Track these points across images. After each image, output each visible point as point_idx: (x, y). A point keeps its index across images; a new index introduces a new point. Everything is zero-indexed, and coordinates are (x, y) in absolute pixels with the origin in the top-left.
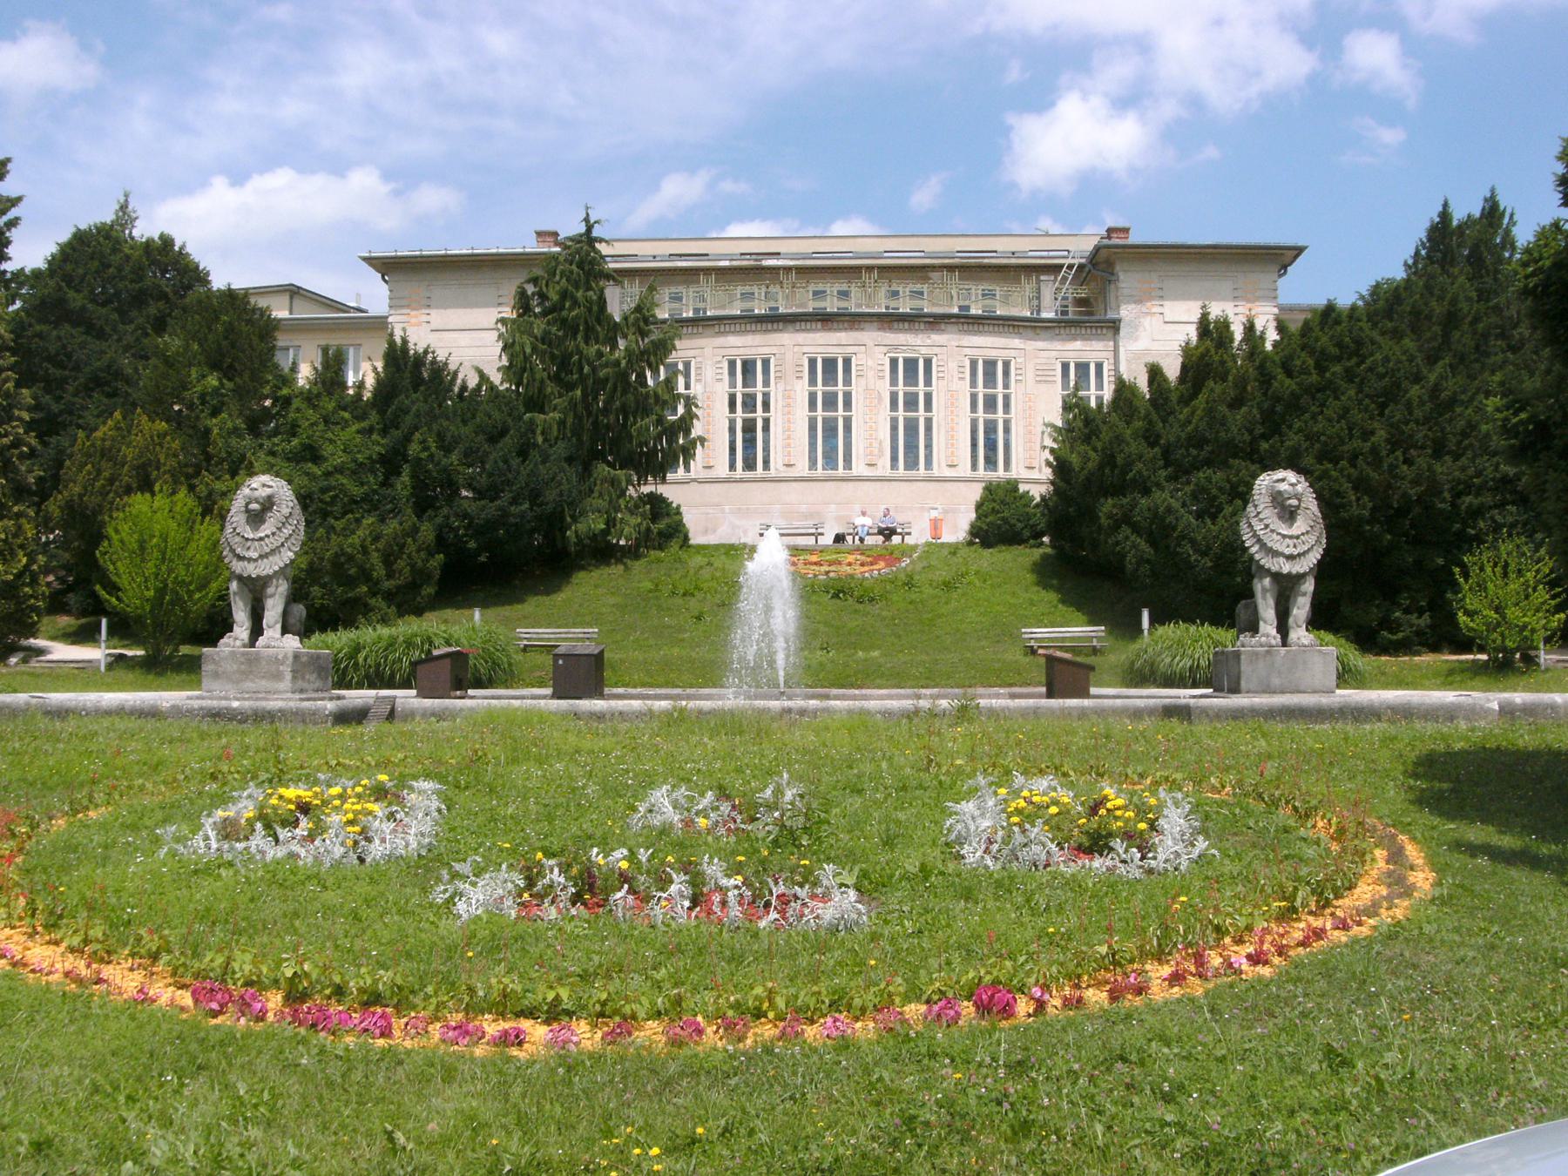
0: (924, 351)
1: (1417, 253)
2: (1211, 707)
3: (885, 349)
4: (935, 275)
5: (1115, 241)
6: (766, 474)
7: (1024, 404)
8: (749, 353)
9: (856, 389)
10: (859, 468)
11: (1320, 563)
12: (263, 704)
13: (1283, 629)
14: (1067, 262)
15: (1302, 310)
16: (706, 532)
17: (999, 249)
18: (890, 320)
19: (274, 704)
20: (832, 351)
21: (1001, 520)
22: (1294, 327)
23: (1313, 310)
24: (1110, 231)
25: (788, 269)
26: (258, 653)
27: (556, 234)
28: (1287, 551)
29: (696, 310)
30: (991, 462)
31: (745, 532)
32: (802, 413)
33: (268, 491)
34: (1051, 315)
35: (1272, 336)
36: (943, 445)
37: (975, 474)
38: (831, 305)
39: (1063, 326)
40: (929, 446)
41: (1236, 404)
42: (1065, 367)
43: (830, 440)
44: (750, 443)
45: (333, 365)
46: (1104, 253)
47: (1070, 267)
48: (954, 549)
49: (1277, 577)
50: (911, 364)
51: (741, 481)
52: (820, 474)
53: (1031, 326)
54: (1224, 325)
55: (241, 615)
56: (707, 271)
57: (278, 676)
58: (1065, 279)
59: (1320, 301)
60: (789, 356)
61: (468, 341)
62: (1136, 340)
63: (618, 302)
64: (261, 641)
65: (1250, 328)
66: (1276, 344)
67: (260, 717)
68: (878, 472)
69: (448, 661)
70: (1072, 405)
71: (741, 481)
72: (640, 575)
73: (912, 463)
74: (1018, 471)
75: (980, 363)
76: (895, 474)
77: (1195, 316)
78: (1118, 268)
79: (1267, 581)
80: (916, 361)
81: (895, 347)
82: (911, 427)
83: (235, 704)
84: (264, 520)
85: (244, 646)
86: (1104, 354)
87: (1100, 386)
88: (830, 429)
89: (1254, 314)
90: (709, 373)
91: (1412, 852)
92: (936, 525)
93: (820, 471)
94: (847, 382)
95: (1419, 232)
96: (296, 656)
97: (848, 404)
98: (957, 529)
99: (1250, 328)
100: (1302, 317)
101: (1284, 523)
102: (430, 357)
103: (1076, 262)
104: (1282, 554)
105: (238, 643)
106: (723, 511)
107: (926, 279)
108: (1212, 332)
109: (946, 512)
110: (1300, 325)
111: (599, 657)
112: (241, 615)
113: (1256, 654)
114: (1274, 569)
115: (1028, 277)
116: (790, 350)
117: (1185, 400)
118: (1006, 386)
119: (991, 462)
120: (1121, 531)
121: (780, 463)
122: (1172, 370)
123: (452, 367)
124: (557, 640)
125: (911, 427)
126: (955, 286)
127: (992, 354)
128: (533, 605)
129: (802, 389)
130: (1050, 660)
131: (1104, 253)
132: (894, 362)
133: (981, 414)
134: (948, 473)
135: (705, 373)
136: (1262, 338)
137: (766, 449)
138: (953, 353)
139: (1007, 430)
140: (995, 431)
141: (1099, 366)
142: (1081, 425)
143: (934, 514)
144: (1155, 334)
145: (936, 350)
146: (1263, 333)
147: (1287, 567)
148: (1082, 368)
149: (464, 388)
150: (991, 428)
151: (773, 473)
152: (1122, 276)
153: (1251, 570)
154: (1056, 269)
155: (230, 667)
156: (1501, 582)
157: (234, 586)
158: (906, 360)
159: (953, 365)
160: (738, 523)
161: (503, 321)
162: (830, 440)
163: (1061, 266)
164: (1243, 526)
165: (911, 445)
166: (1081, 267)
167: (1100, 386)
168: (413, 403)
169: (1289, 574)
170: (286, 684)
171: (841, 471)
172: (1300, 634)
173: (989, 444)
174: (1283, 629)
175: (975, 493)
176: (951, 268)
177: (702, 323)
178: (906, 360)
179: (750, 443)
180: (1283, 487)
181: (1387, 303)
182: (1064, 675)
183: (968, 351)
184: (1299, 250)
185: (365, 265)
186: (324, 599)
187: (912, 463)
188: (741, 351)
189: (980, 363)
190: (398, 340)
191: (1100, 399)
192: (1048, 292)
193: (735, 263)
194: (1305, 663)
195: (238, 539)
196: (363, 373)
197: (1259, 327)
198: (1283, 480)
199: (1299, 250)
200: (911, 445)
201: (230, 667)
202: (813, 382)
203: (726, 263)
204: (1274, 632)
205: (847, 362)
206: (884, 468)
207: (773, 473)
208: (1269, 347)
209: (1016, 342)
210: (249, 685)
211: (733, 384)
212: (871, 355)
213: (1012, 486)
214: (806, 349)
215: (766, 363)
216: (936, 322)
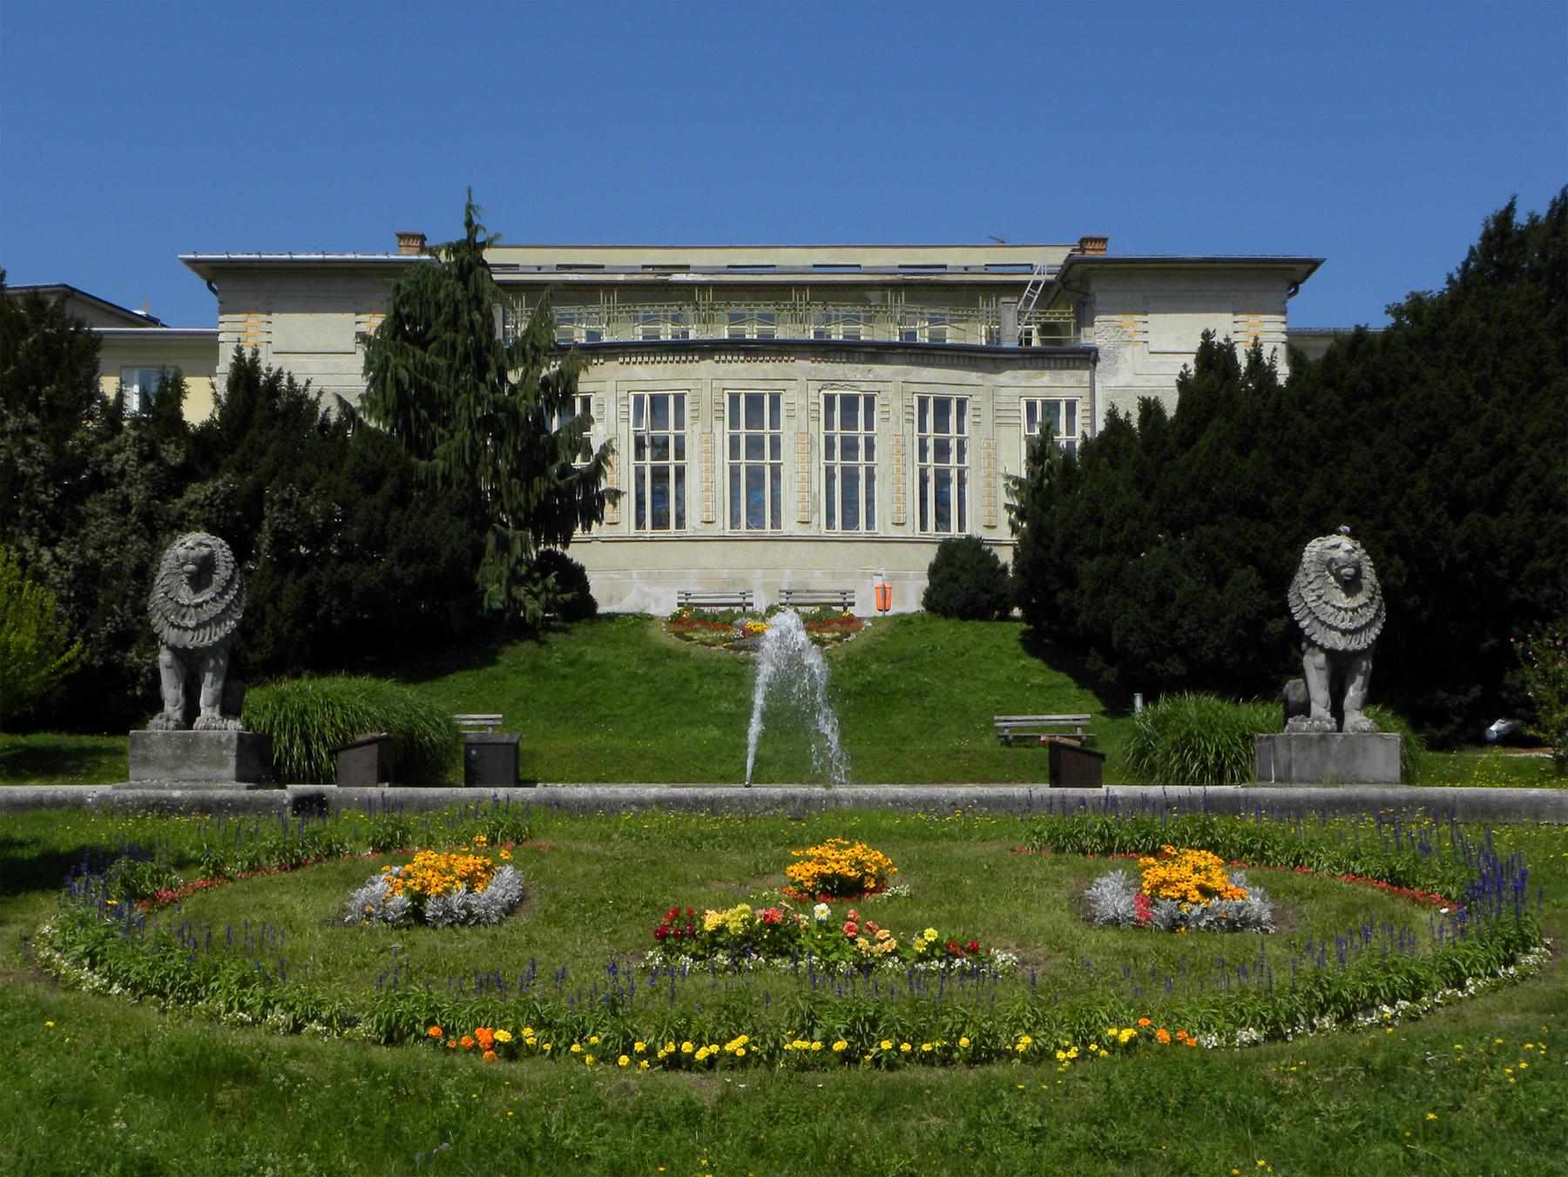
0: (864, 387)
1: (1466, 264)
2: (1262, 797)
3: (819, 385)
4: (874, 295)
5: (1090, 254)
6: (680, 532)
7: (990, 447)
8: (660, 388)
9: (787, 430)
10: (789, 526)
11: (1380, 639)
12: (211, 793)
13: (1337, 711)
14: (1032, 278)
15: (1322, 335)
16: (610, 600)
17: (950, 263)
18: (823, 349)
19: (218, 793)
20: (757, 387)
21: (961, 582)
22: (1315, 354)
23: (1336, 335)
24: (1083, 241)
25: (703, 286)
26: (196, 736)
27: (423, 238)
28: (1342, 626)
29: (590, 334)
30: (942, 520)
31: (657, 601)
32: (723, 460)
33: (205, 551)
34: (1015, 345)
35: (1283, 372)
36: (909, 484)
37: (924, 535)
38: (751, 332)
39: (1025, 357)
40: (870, 501)
41: (1243, 449)
42: (1031, 407)
43: (754, 494)
44: (660, 503)
45: (166, 400)
46: (1078, 268)
47: (1036, 285)
48: (904, 621)
49: (1331, 654)
50: (849, 403)
51: (652, 540)
52: (770, 510)
53: (989, 358)
54: (1228, 351)
55: (171, 691)
56: (609, 287)
57: (221, 763)
58: (1028, 300)
59: (1347, 325)
60: (706, 393)
61: (325, 357)
62: (1115, 373)
63: (512, 325)
64: (199, 722)
65: (1255, 356)
66: (1290, 381)
67: (205, 806)
68: (812, 531)
69: (374, 749)
70: (1039, 452)
71: (652, 540)
72: (562, 646)
73: (850, 521)
74: (974, 529)
75: (931, 402)
76: (832, 534)
77: (1196, 343)
78: (1093, 287)
79: (1321, 658)
80: (855, 399)
81: (831, 382)
82: (850, 477)
83: (177, 794)
84: (190, 589)
85: (178, 727)
86: (1077, 392)
87: (1070, 429)
88: (755, 476)
89: (1259, 335)
90: (610, 411)
91: (237, 580)
92: (884, 593)
93: (743, 530)
94: (775, 423)
95: (1474, 237)
96: (241, 737)
97: (775, 452)
98: (910, 599)
99: (1255, 356)
100: (1327, 343)
101: (1333, 591)
102: (285, 381)
103: (1043, 278)
104: (1336, 629)
105: (172, 724)
106: (630, 577)
107: (865, 301)
108: (1213, 357)
109: (891, 578)
110: (1321, 355)
111: (516, 745)
112: (171, 691)
113: (1310, 739)
114: (1327, 645)
115: (988, 299)
116: (707, 383)
117: (1187, 443)
118: (960, 429)
119: (942, 520)
120: (1127, 587)
121: (698, 520)
122: (1170, 405)
123: (312, 395)
124: (1035, 729)
125: (850, 477)
126: (899, 305)
127: (945, 391)
128: (462, 680)
129: (722, 431)
130: (1055, 748)
131: (1078, 268)
132: (829, 400)
133: (648, 462)
134: (895, 533)
135: (610, 403)
136: (1272, 375)
137: (680, 500)
138: (895, 390)
139: (962, 482)
140: (948, 481)
141: (1071, 406)
142: (1051, 484)
143: (878, 582)
144: (1144, 360)
145: (879, 386)
146: (1272, 366)
147: (1341, 644)
148: (1051, 407)
149: (325, 418)
150: (942, 479)
151: (689, 531)
152: (1099, 298)
153: (1295, 638)
154: (1016, 288)
155: (164, 751)
156: (1559, 662)
157: (165, 657)
158: (843, 397)
159: (897, 404)
160: (647, 589)
161: (363, 338)
162: (754, 494)
163: (1025, 284)
164: (1292, 597)
165: (849, 499)
166: (1048, 284)
167: (1070, 429)
168: (270, 442)
169: (1345, 651)
170: (230, 770)
171: (768, 530)
172: (1356, 719)
173: (940, 495)
174: (1337, 711)
175: (930, 554)
176: (895, 287)
177: (598, 350)
178: (843, 397)
179: (660, 496)
180: (1339, 554)
181: (1423, 322)
182: (1070, 763)
183: (917, 388)
184: (1314, 264)
185: (187, 269)
186: (245, 664)
187: (850, 521)
188: (650, 386)
189: (931, 402)
190: (248, 355)
191: (1070, 444)
192: (1009, 316)
193: (636, 277)
194: (1365, 749)
195: (170, 605)
196: (200, 404)
197: (1266, 353)
198: (1337, 547)
199: (1314, 264)
200: (849, 499)
201: (164, 751)
202: (734, 423)
203: (621, 278)
204: (1328, 715)
205: (775, 400)
206: (819, 527)
207: (689, 531)
208: (1281, 380)
209: (973, 377)
210: (186, 772)
211: (922, 427)
212: (801, 389)
213: (974, 545)
214: (726, 384)
215: (679, 400)
216: (879, 353)
